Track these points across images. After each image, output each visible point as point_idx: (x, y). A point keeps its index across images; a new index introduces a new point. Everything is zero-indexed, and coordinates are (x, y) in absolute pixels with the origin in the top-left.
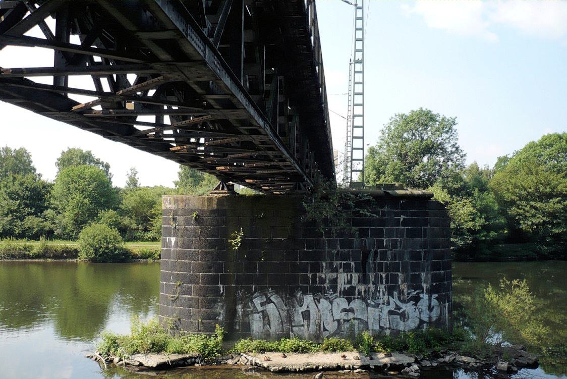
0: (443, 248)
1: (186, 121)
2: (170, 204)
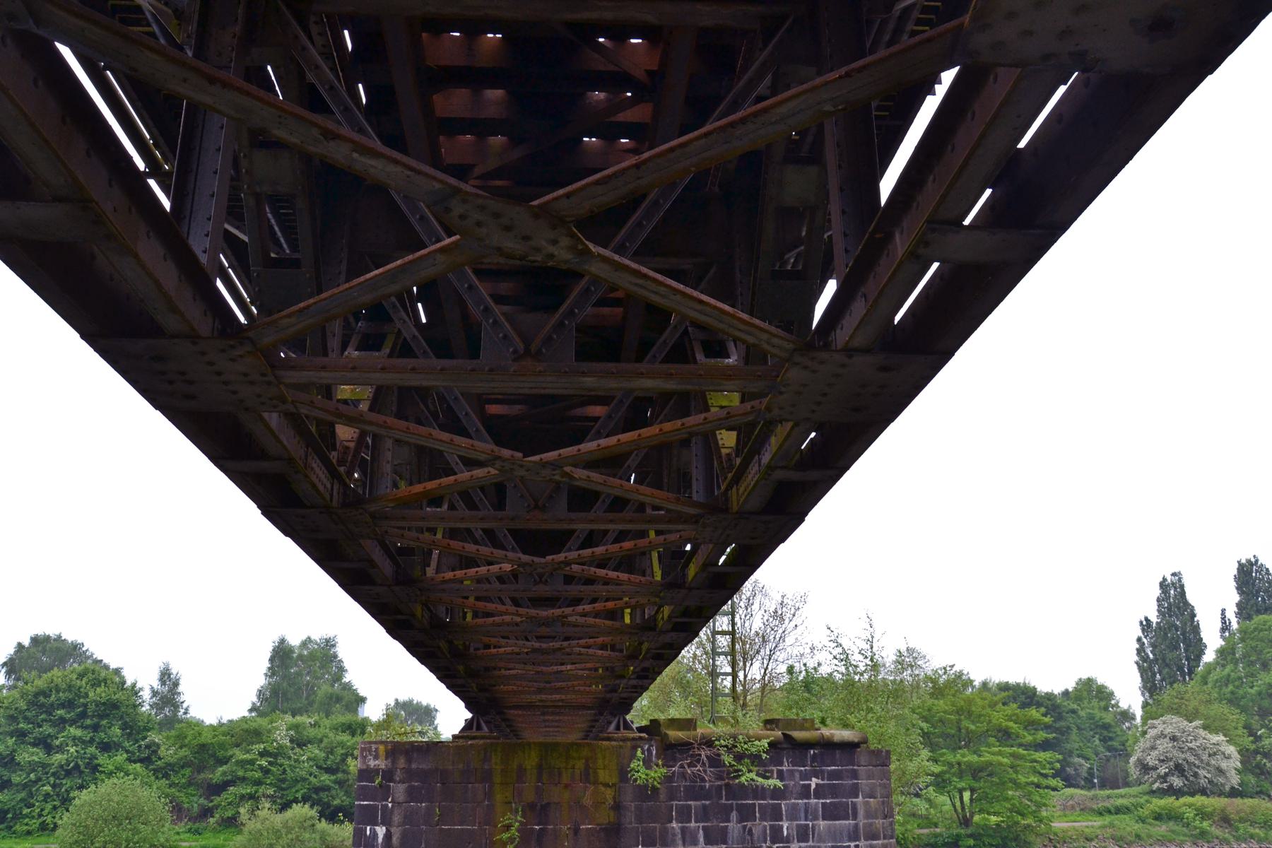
0: (884, 838)
1: (595, 549)
2: (376, 757)
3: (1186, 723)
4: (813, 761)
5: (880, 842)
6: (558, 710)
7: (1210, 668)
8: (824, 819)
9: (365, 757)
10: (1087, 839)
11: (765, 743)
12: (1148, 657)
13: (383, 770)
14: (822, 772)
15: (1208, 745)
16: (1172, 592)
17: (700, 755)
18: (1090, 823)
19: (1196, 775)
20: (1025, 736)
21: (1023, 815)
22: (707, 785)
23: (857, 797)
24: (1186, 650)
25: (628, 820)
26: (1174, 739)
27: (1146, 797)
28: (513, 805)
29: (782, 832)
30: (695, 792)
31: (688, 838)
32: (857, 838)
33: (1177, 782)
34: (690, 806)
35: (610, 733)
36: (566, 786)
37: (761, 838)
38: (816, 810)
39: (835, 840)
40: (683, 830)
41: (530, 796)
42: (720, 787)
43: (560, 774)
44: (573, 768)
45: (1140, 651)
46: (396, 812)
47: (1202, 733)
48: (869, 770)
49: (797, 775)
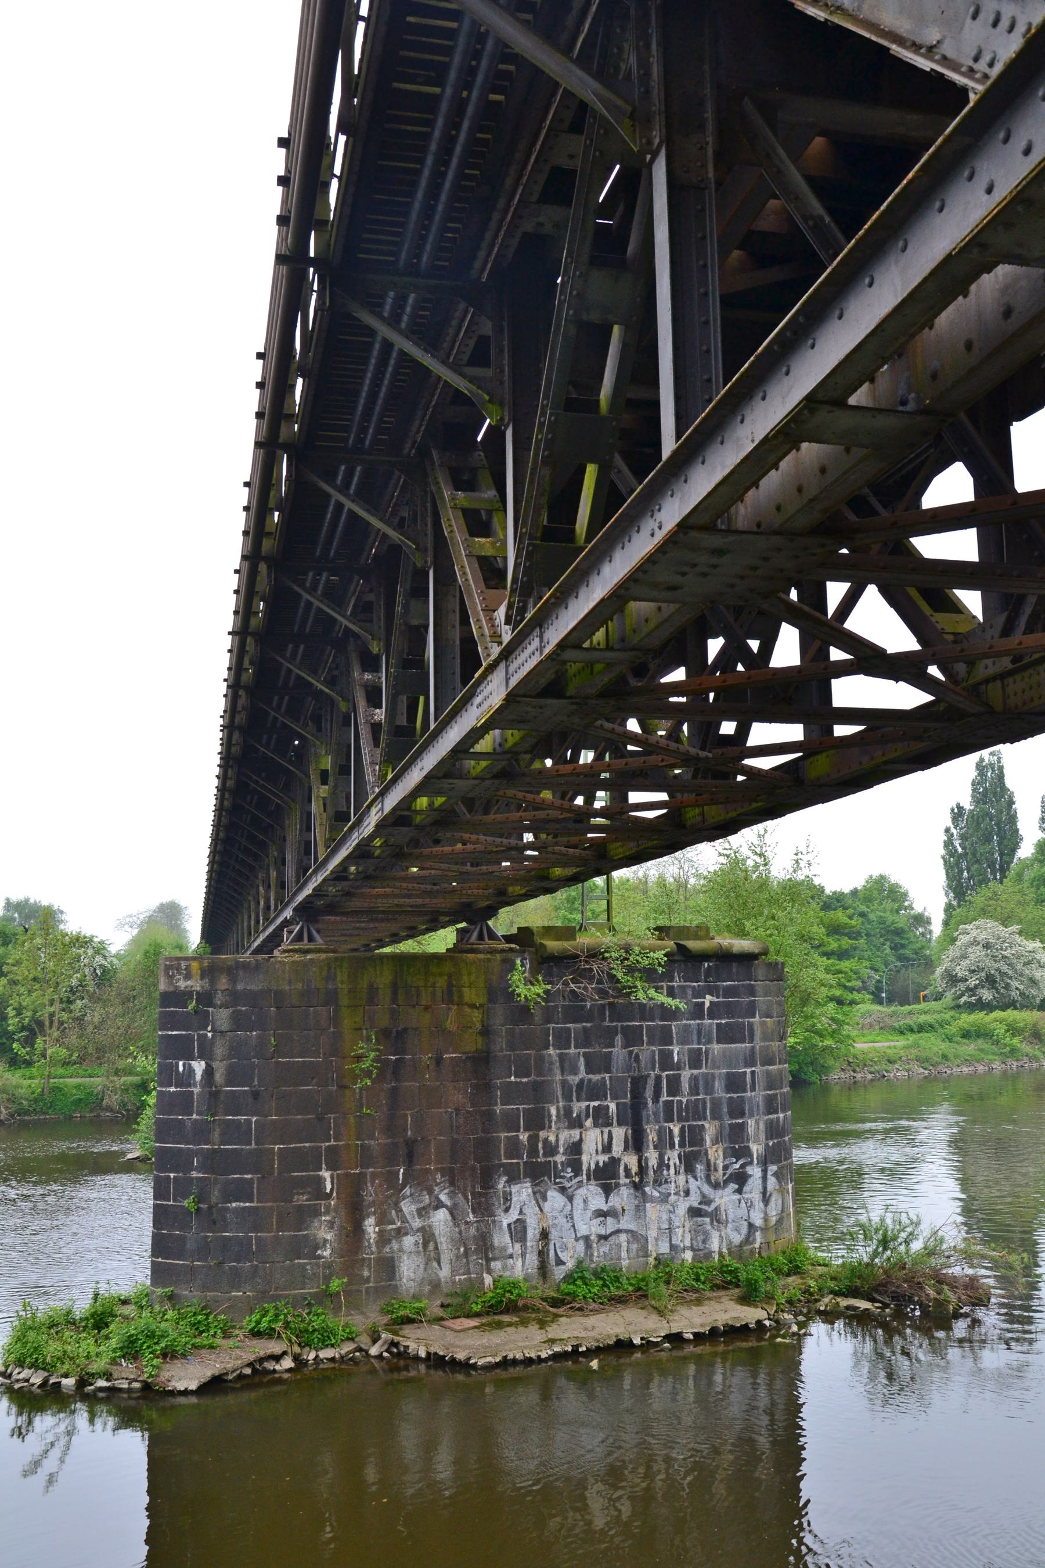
0: (780, 1063)
2: (188, 977)
3: (1001, 928)
4: (707, 975)
5: (775, 1067)
6: (390, 917)
7: (1025, 864)
8: (718, 1042)
9: (172, 977)
10: (890, 1061)
11: (660, 954)
12: (956, 851)
13: (198, 993)
14: (717, 988)
15: (1024, 953)
16: (989, 774)
17: (591, 970)
18: (892, 1044)
19: (1007, 987)
20: (829, 943)
21: (821, 1036)
22: (588, 1004)
23: (754, 1016)
24: (1000, 843)
25: (498, 1047)
26: (987, 946)
27: (952, 1013)
28: (364, 1032)
29: (673, 1057)
30: (575, 1013)
31: (567, 1065)
32: (753, 1064)
33: (987, 995)
34: (569, 1029)
35: (473, 944)
36: (426, 1008)
37: (649, 1066)
38: (710, 1032)
39: (729, 1066)
40: (561, 1057)
41: (384, 1021)
42: (603, 1006)
43: (418, 996)
44: (434, 986)
45: (948, 844)
46: (219, 1043)
47: (1018, 939)
48: (766, 985)
49: (690, 992)
